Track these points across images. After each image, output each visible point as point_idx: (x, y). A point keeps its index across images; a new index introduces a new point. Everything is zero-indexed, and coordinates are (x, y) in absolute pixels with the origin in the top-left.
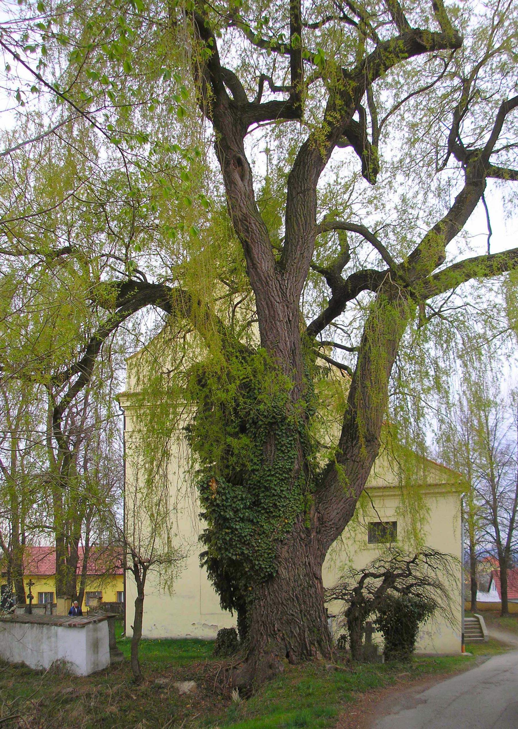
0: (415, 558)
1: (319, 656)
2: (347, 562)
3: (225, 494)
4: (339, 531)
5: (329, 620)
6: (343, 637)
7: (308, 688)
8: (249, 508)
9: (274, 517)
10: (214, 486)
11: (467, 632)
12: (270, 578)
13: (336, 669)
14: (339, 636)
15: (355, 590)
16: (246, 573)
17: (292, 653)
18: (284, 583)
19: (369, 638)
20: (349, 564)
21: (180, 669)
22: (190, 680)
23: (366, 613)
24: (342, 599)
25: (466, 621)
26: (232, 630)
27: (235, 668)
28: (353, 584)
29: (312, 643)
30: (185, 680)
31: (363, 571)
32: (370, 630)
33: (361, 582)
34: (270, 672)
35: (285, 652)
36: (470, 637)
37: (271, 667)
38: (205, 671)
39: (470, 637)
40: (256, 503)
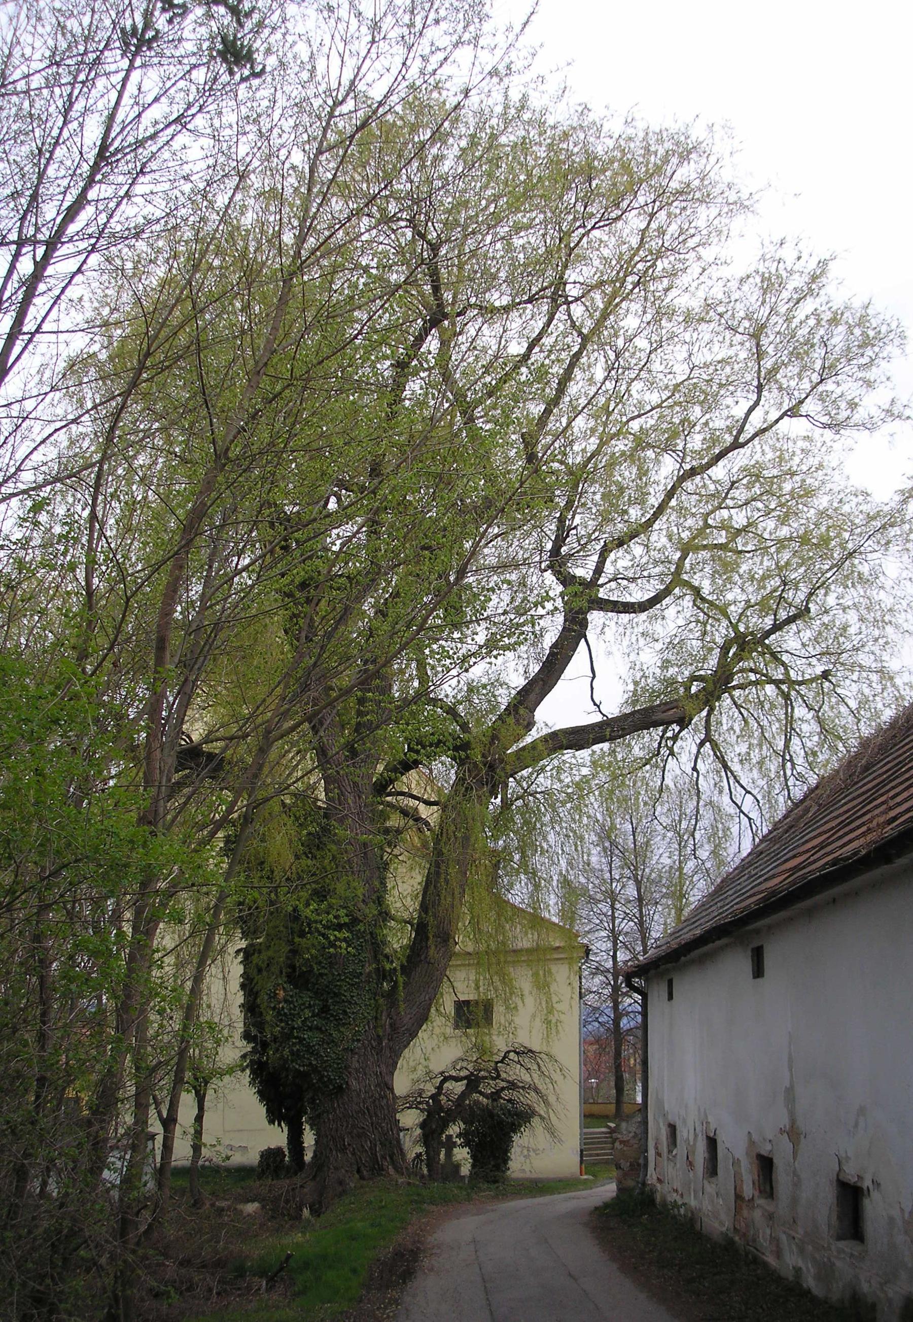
0: (504, 1058)
1: (391, 1170)
2: (423, 1061)
3: (292, 1002)
4: (413, 1035)
5: (402, 1134)
6: (419, 1155)
7: (381, 1201)
8: (318, 1015)
9: (344, 1024)
10: (281, 994)
11: (586, 1150)
12: (340, 1090)
13: (409, 1184)
14: (414, 1155)
15: (432, 1097)
16: (313, 1084)
17: (362, 1168)
18: (354, 1094)
19: (449, 1154)
20: (425, 1063)
21: (241, 1191)
22: (253, 1201)
23: (445, 1126)
24: (417, 1108)
25: (586, 1134)
26: (279, 1150)
27: (301, 1186)
28: (430, 1089)
29: (384, 1157)
30: (248, 1201)
31: (442, 1073)
32: (450, 1145)
33: (440, 1088)
34: (340, 1189)
35: (355, 1167)
36: (591, 1155)
37: (341, 1183)
38: (270, 1191)
39: (591, 1155)
40: (325, 1009)
